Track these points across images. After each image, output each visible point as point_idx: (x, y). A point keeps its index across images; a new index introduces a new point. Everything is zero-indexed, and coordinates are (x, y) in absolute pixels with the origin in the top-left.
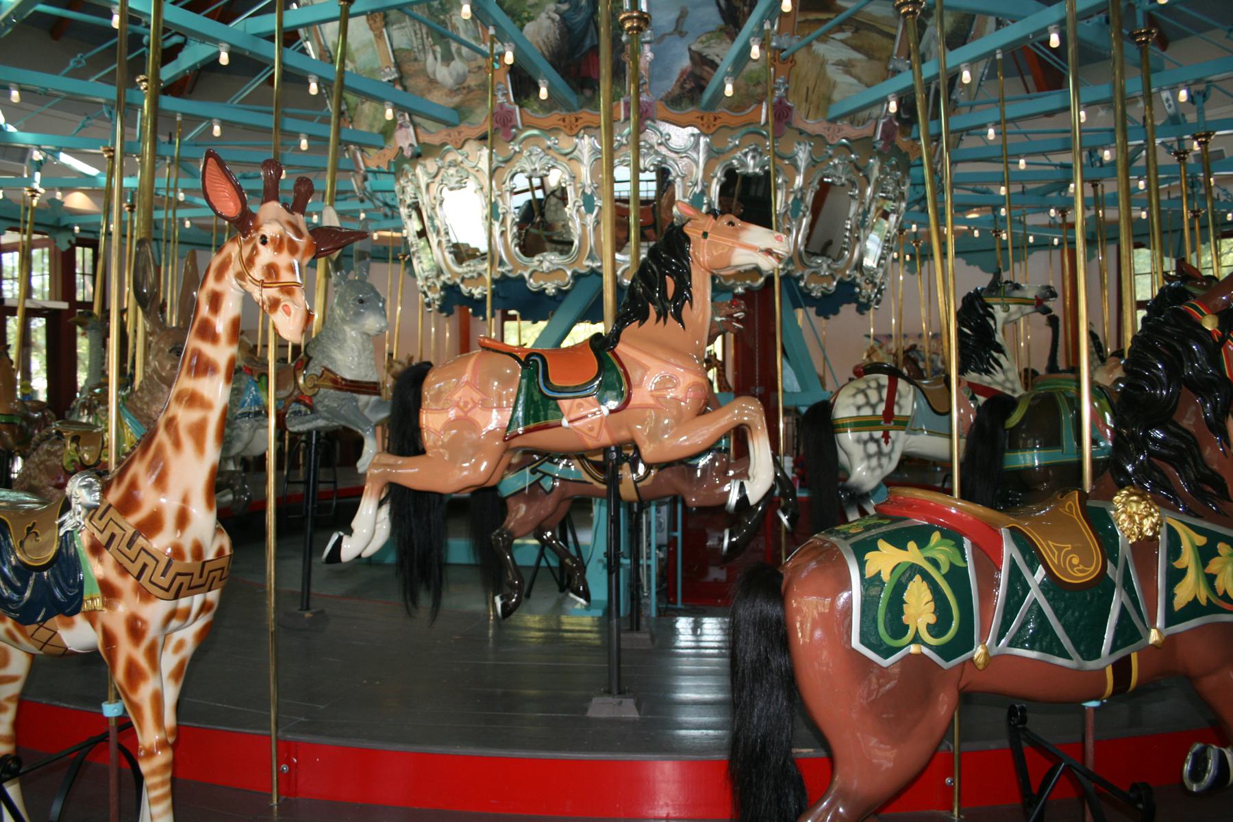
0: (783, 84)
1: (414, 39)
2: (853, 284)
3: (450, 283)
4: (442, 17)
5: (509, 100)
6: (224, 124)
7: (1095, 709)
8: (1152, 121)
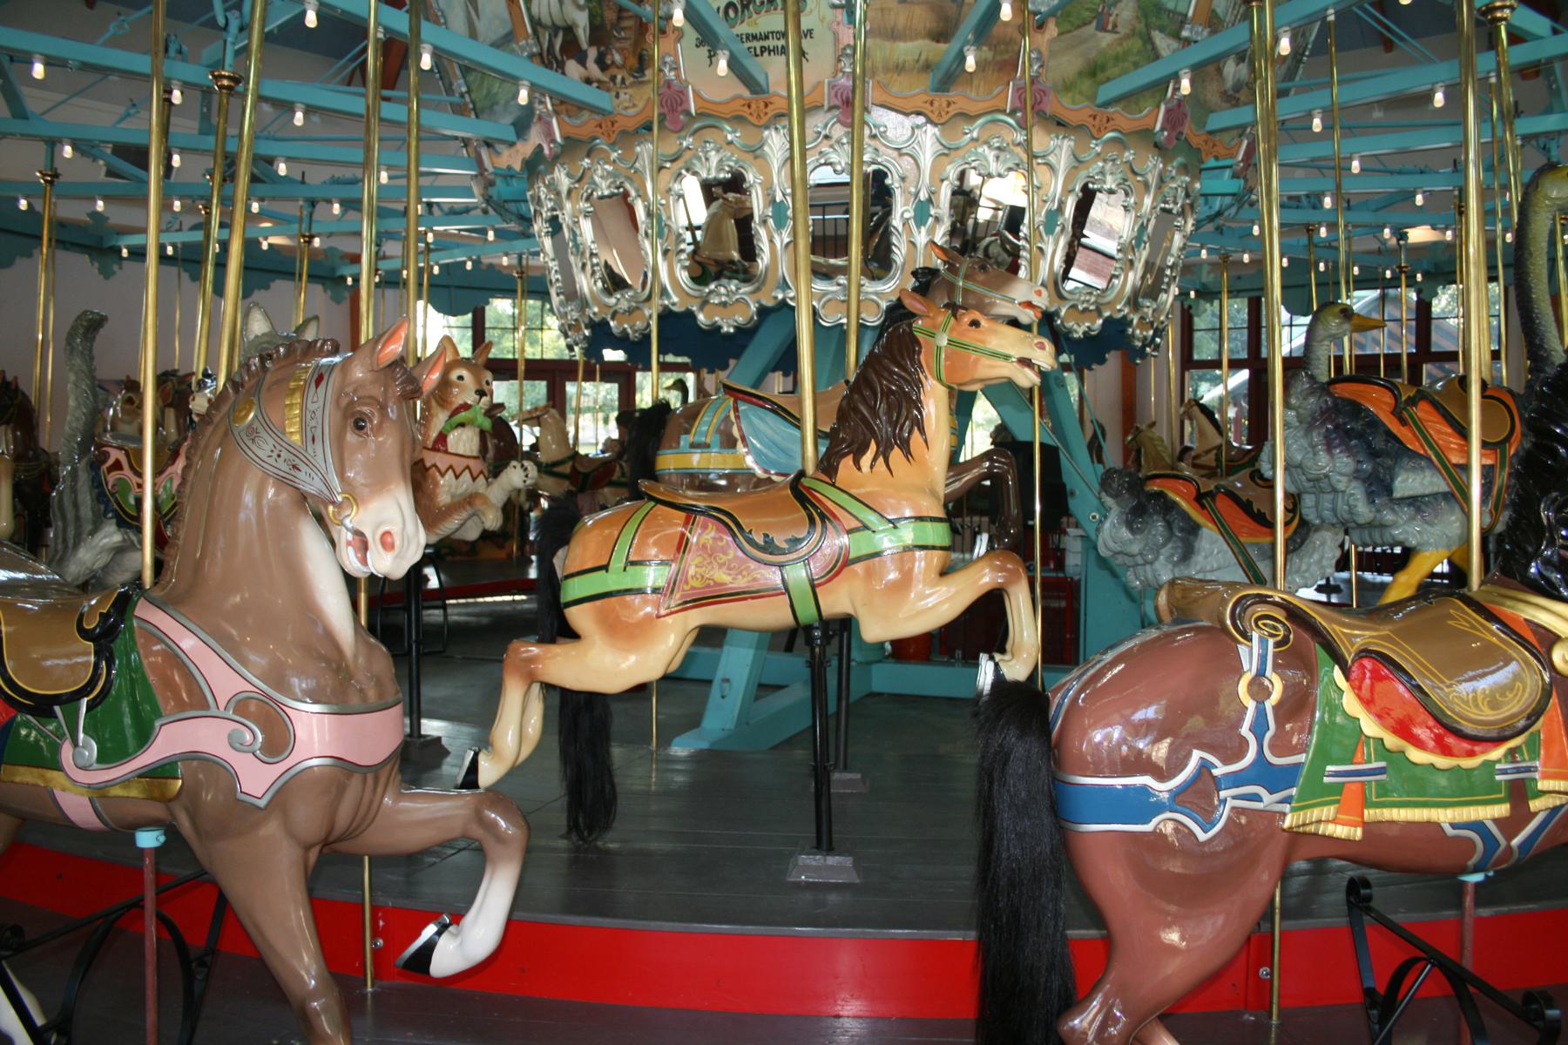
2: (1125, 322)
3: (596, 319)
6: (309, 110)
7: (1477, 885)
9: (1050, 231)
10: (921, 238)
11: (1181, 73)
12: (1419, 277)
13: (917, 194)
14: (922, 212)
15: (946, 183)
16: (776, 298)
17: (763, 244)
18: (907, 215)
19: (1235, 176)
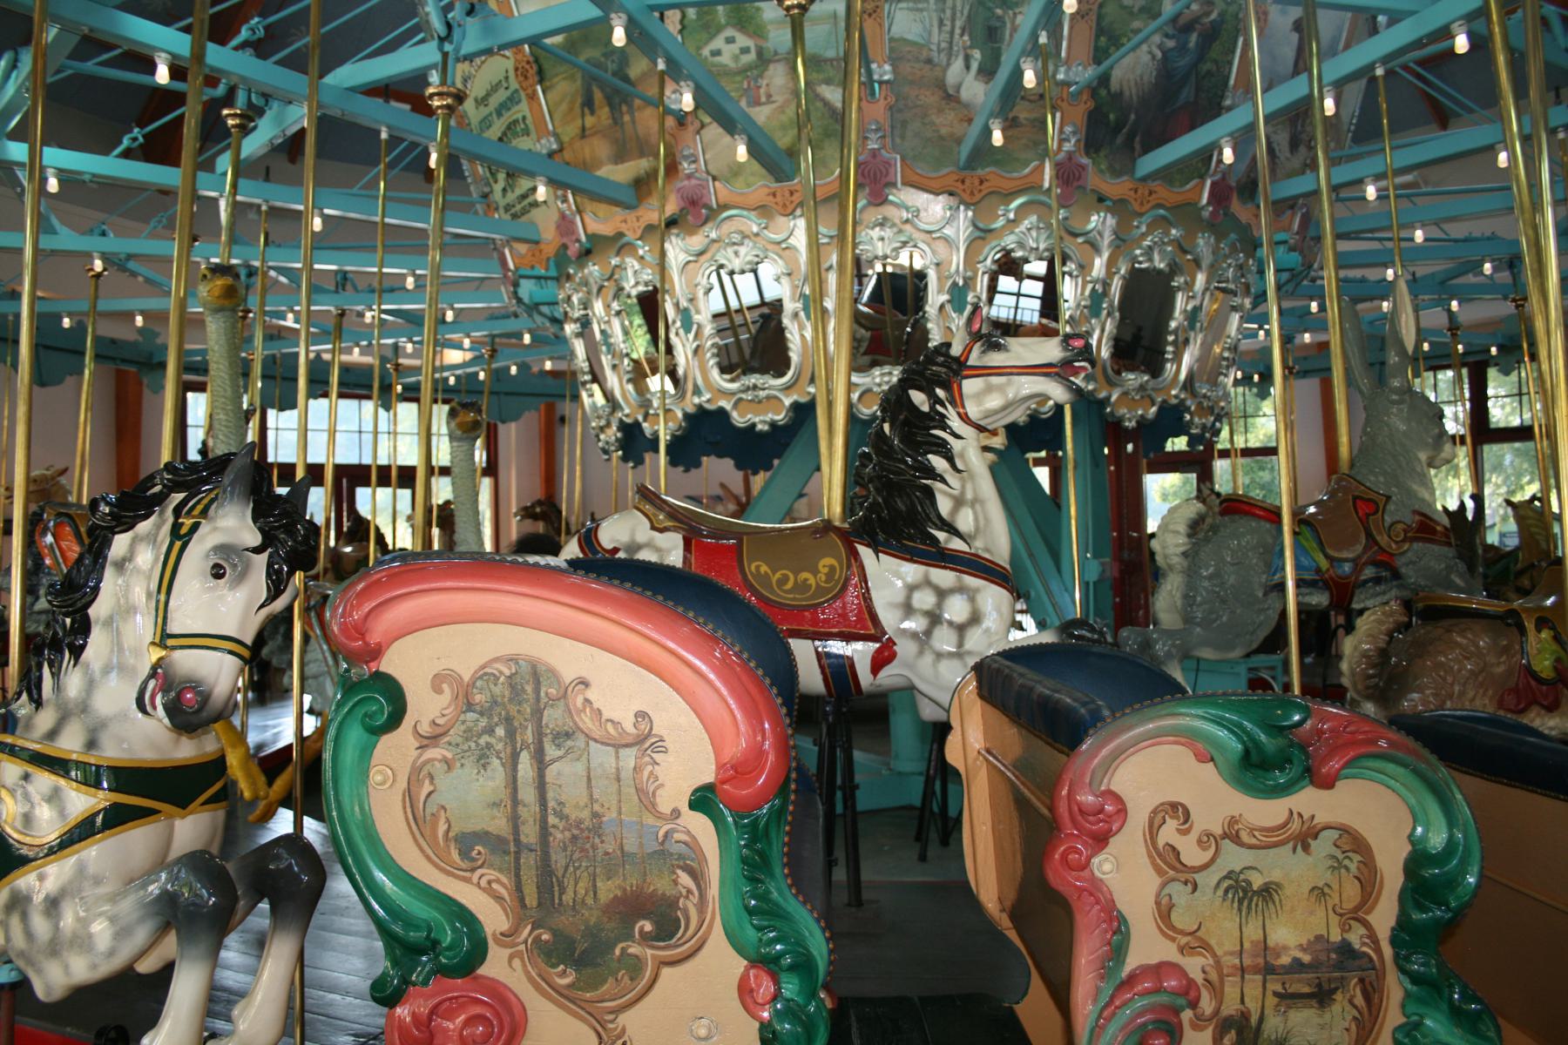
0: (1074, 133)
1: (935, 30)
4: (999, 11)
5: (569, 206)
8: (537, 691)
9: (1096, 314)
11: (1223, 141)
12: (1256, 378)
19: (1292, 249)
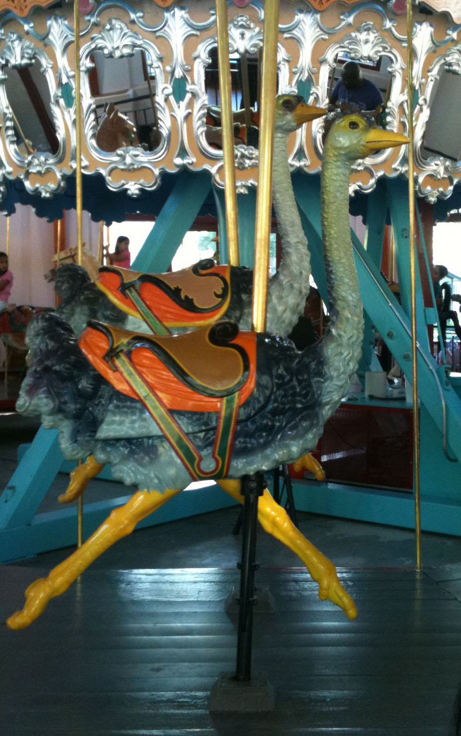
3: (11, 177)
10: (181, 112)
13: (173, 73)
14: (179, 89)
15: (198, 60)
16: (72, 167)
17: (59, 123)
18: (167, 92)
